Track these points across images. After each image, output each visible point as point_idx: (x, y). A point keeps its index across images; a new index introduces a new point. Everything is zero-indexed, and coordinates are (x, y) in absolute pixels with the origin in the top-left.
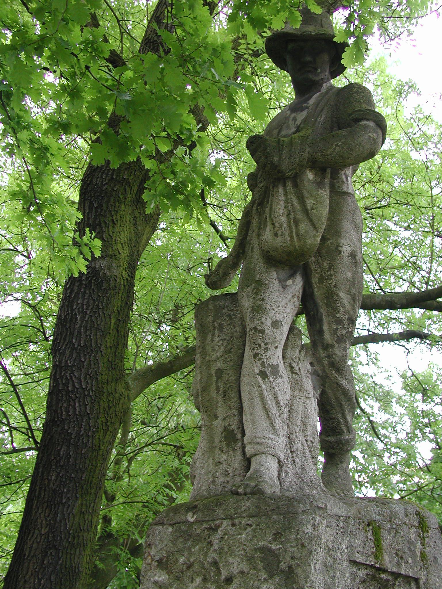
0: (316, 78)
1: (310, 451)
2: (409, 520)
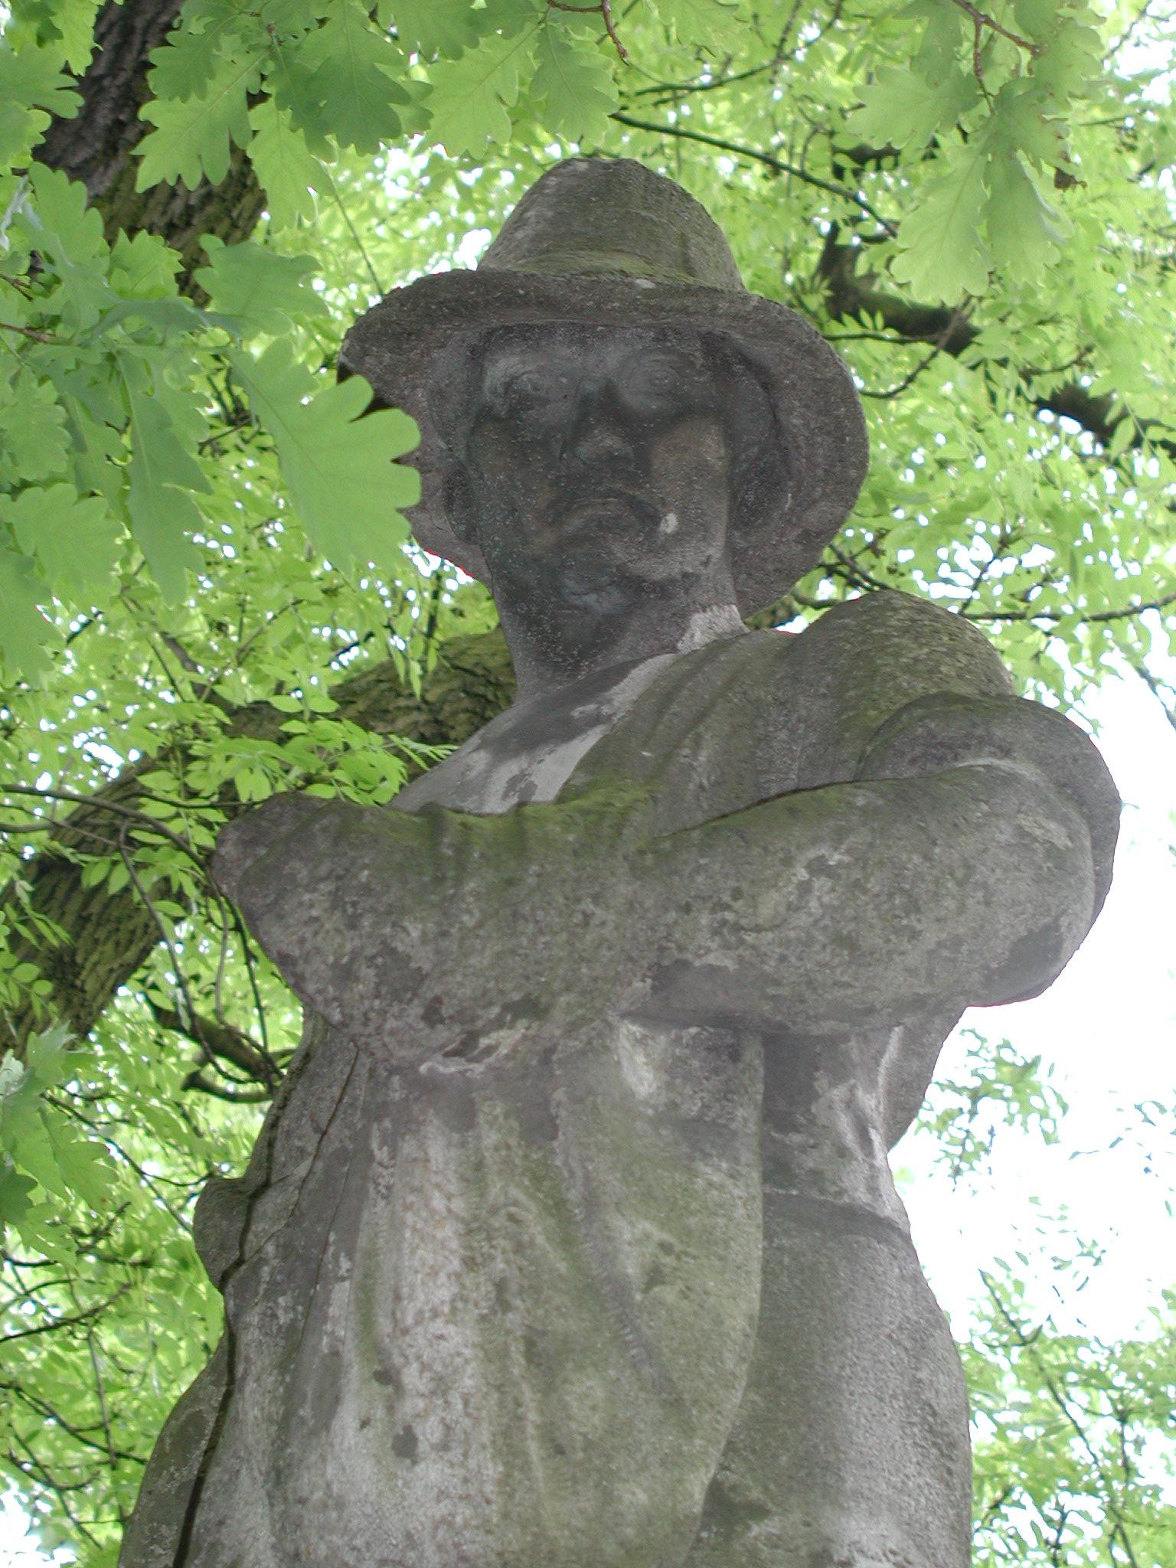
0: (659, 570)
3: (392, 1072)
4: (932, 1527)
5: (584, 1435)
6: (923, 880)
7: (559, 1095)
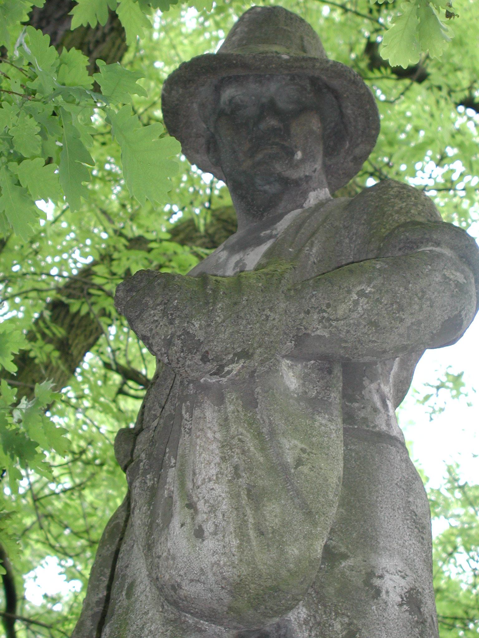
0: (294, 174)
3: (189, 383)
4: (416, 561)
5: (272, 527)
6: (405, 298)
7: (258, 390)
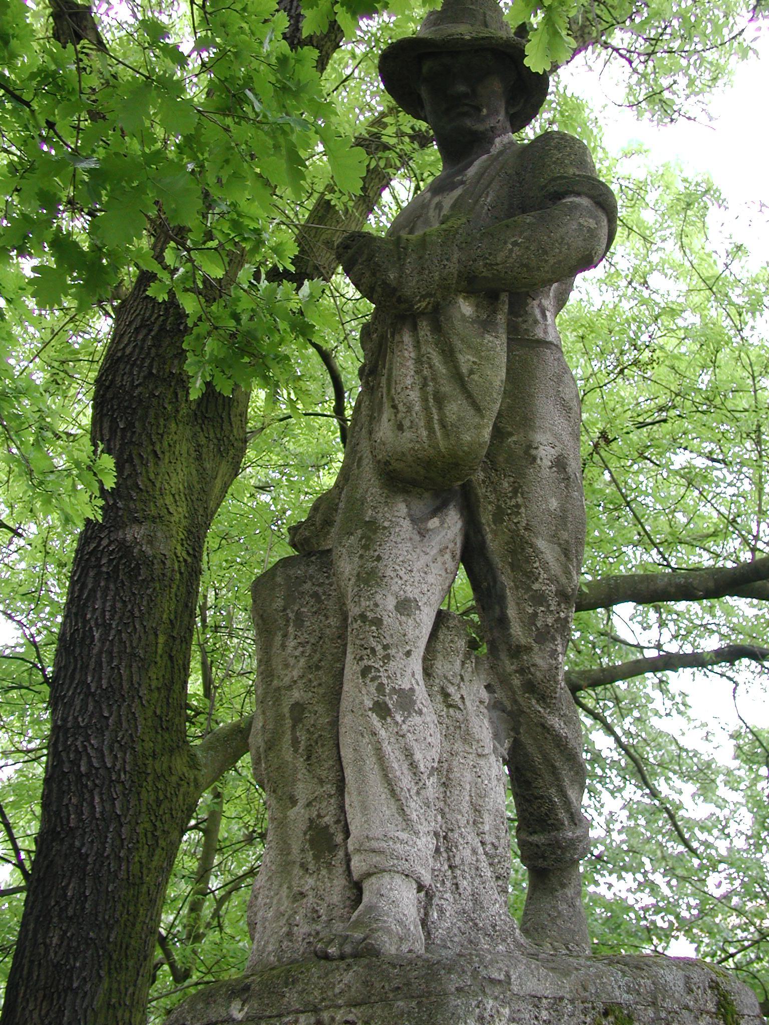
0: (480, 127)
1: (491, 864)
2: (696, 1000)
